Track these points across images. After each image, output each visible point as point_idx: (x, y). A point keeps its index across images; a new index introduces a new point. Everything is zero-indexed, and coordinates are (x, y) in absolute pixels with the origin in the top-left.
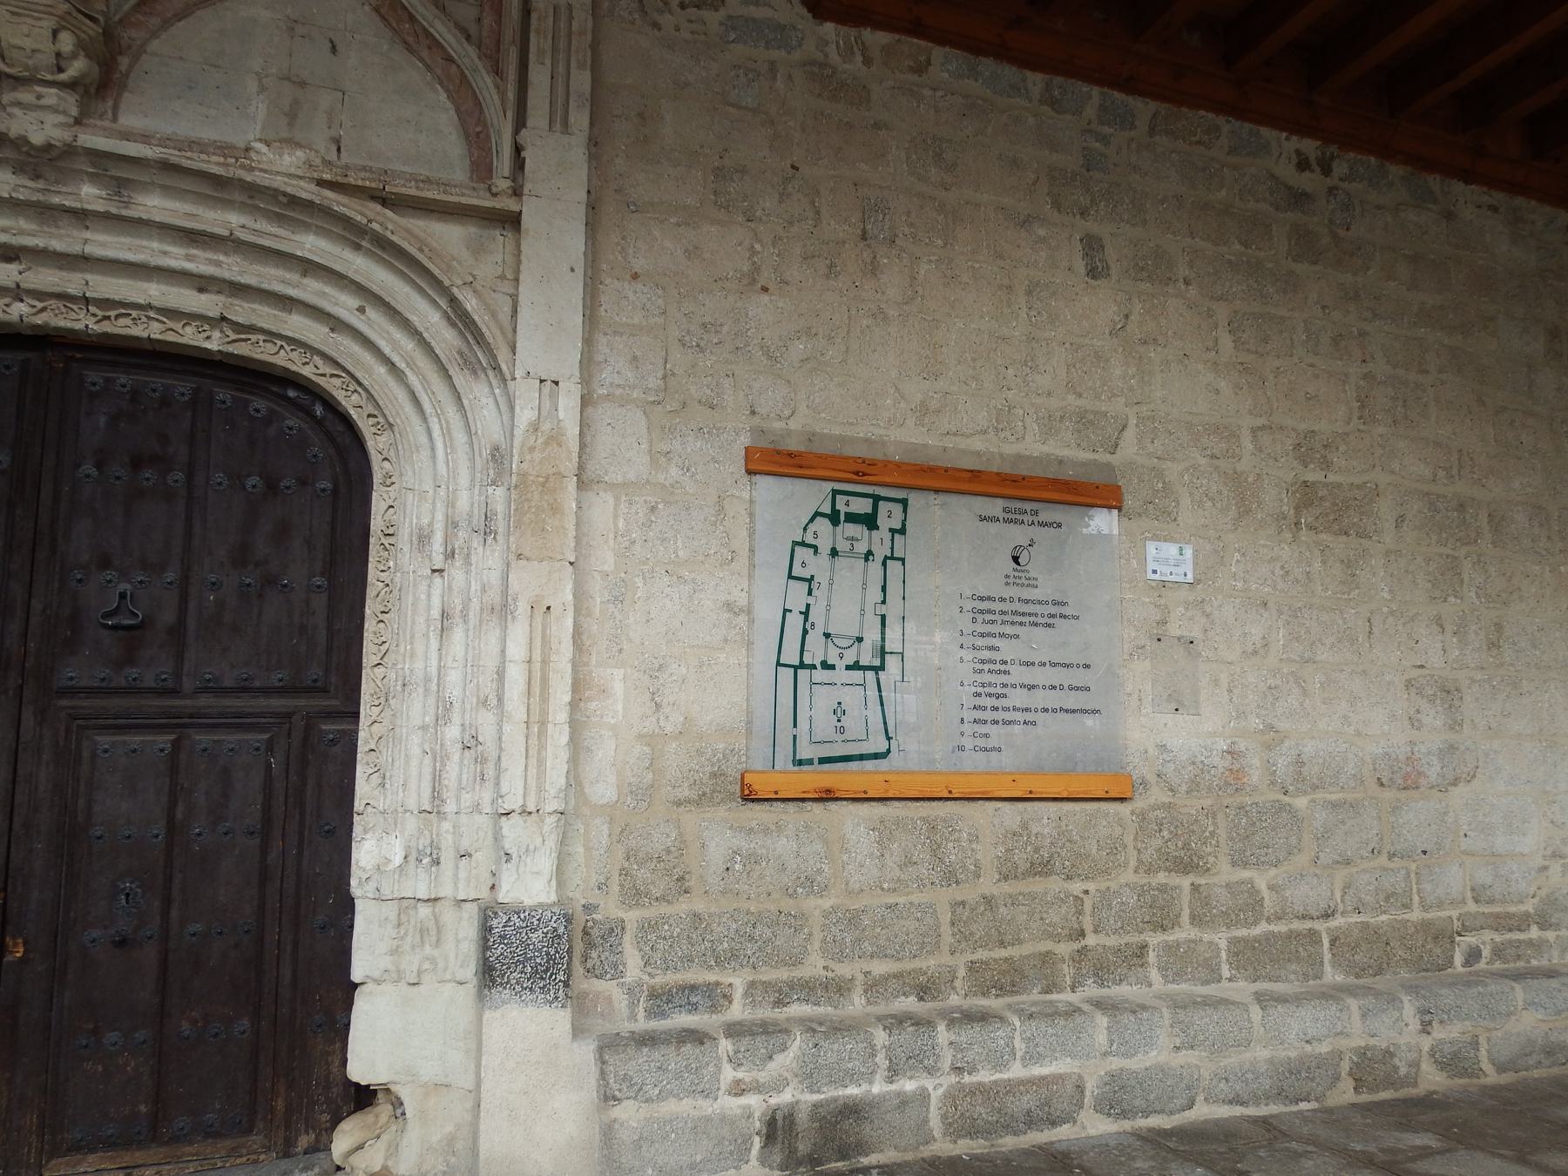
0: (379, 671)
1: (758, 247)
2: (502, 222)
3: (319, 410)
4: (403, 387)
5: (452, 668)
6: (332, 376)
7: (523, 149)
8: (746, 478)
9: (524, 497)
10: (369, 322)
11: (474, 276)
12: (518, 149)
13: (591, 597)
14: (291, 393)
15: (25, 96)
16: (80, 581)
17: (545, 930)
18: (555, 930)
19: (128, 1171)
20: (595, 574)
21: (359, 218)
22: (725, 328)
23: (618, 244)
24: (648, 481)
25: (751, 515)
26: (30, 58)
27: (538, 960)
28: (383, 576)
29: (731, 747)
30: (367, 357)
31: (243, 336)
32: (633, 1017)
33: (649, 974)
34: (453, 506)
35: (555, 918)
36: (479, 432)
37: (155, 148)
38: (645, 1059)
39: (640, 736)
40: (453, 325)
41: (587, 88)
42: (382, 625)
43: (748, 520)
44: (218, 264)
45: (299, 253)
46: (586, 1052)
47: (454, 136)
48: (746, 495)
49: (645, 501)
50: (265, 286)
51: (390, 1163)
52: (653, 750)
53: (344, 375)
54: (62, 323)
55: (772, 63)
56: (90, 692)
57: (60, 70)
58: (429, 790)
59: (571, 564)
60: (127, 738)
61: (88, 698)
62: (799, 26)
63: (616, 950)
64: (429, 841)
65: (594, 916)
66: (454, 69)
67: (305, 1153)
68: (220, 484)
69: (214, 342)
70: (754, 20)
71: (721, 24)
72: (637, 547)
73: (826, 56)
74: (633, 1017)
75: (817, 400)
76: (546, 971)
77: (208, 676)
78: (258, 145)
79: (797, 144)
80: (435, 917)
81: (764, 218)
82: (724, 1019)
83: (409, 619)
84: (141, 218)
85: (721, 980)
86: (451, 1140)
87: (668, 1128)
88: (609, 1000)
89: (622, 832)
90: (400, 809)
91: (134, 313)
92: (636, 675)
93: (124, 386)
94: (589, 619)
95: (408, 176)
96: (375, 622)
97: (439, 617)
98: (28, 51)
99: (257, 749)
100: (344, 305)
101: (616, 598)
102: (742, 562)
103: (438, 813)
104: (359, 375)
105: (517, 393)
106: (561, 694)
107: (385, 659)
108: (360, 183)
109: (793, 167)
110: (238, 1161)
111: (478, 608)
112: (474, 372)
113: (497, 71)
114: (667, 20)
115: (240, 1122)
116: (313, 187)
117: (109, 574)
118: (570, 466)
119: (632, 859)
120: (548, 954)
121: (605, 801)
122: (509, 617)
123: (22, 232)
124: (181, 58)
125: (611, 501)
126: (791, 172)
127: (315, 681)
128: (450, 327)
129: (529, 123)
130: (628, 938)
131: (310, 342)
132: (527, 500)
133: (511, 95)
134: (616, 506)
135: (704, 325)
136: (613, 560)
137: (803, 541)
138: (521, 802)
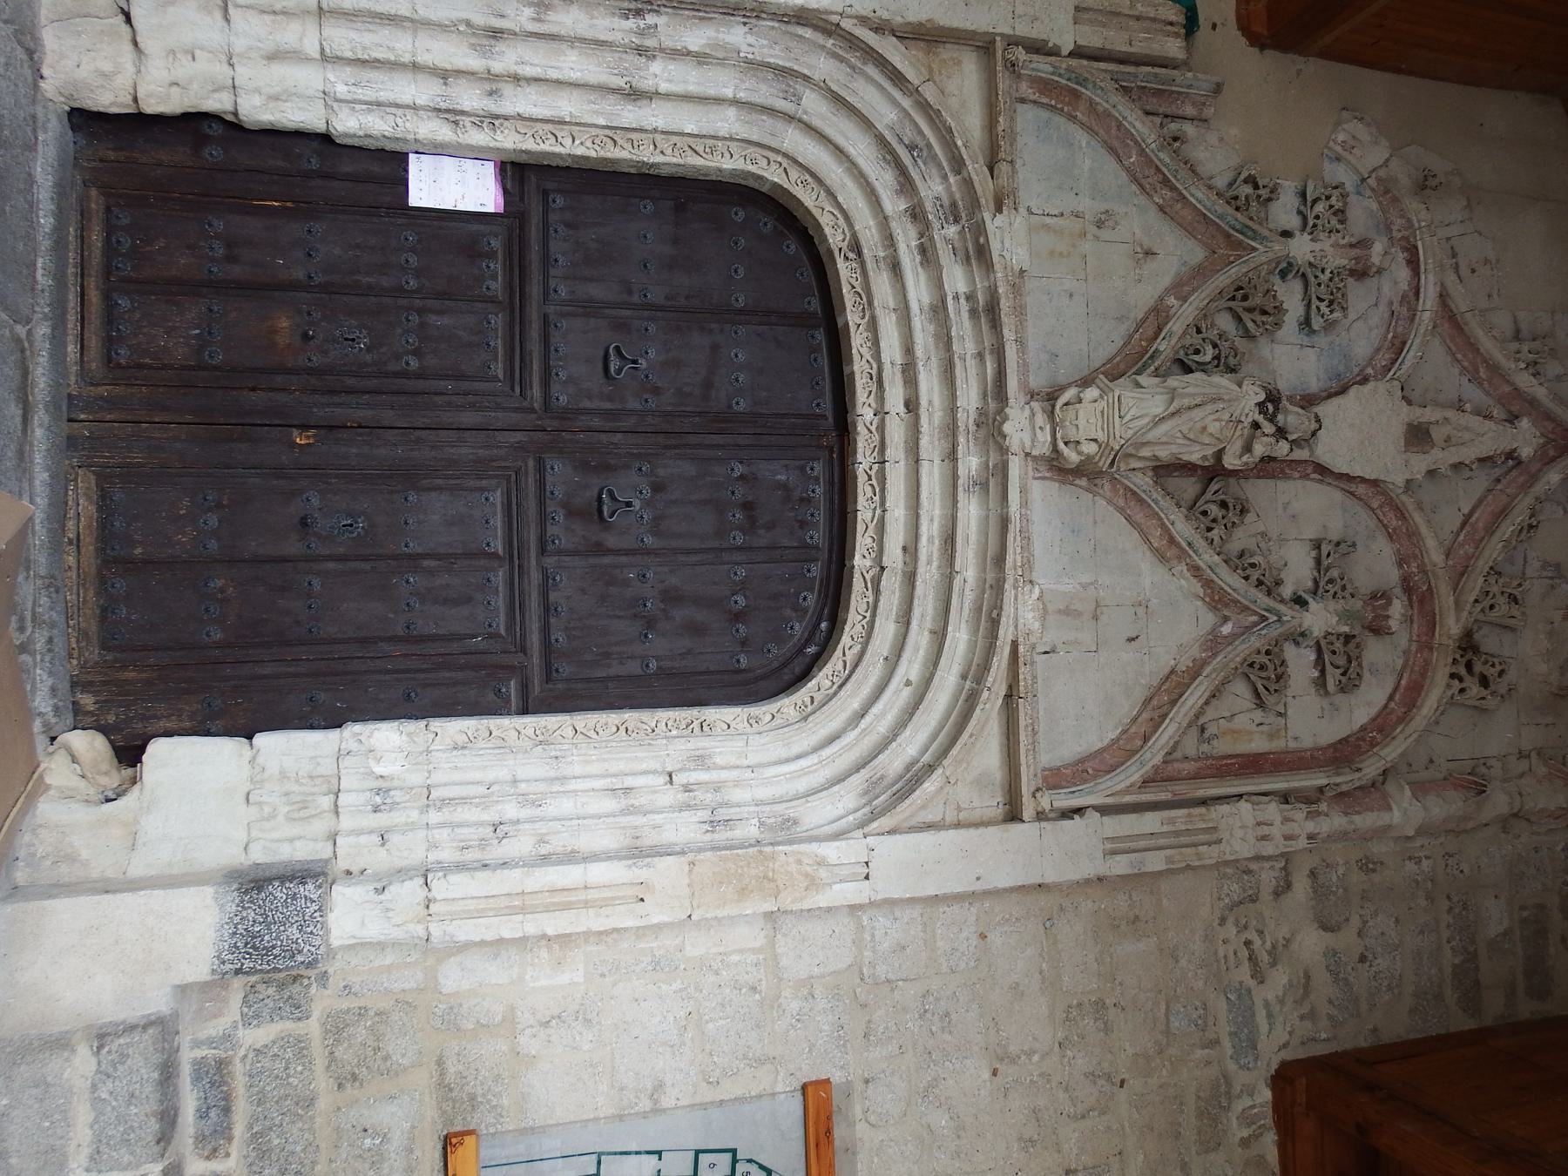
0: (569, 732)
1: (1036, 1058)
2: (1011, 801)
3: (811, 650)
4: (843, 725)
5: (575, 802)
6: (845, 662)
7: (1082, 816)
8: (798, 1086)
9: (751, 860)
10: (898, 692)
11: (956, 783)
12: (1079, 811)
13: (656, 938)
14: (824, 625)
15: (1040, 419)
16: (640, 469)
17: (300, 941)
18: (300, 952)
19: (75, 542)
20: (681, 938)
21: (990, 679)
22: (947, 1037)
23: (1011, 915)
24: (781, 979)
25: (760, 1097)
26: (1070, 423)
27: (267, 938)
28: (662, 726)
29: (504, 1113)
30: (866, 691)
31: (869, 585)
32: (197, 1044)
33: (246, 1056)
34: (735, 786)
35: (313, 949)
36: (809, 805)
37: (1018, 512)
38: (145, 1077)
39: (512, 1009)
40: (908, 768)
41: (1150, 868)
42: (615, 729)
43: (753, 1094)
44: (929, 563)
45: (950, 629)
46: (158, 1002)
47: (1079, 749)
48: (780, 1088)
49: (760, 980)
50: (916, 602)
51: (52, 792)
52: (497, 1025)
53: (847, 672)
54: (860, 445)
55: (1216, 1042)
56: (541, 484)
57: (1066, 443)
58: (451, 796)
59: (690, 916)
60: (499, 515)
61: (536, 481)
62: (1259, 1063)
63: (276, 1014)
64: (398, 800)
65: (315, 985)
66: (1140, 743)
67: (74, 703)
68: (736, 574)
69: (861, 561)
70: (1253, 1015)
71: (1241, 983)
72: (712, 978)
73: (1239, 1097)
74: (197, 1044)
75: (890, 1150)
76: (254, 947)
77: (558, 578)
78: (1037, 591)
79: (1146, 1082)
80: (320, 813)
81: (1066, 1060)
82: (187, 1154)
83: (621, 755)
84: (958, 502)
85: (235, 1143)
86: (72, 858)
87: (57, 1117)
88: (218, 1014)
89: (407, 1003)
90: (431, 767)
91: (877, 498)
92: (579, 996)
93: (813, 491)
94: (633, 938)
95: (1035, 715)
96: (617, 722)
97: (625, 786)
98: (1076, 422)
99: (490, 626)
100: (911, 668)
101: (658, 963)
102: (710, 1095)
103: (428, 806)
104: (848, 686)
105: (852, 842)
106: (553, 924)
107: (581, 736)
108: (1021, 677)
109: (1122, 1083)
110: (73, 640)
111: (637, 824)
112: (866, 792)
113: (1146, 782)
114: (1231, 930)
115: (116, 639)
116: (1010, 638)
117: (648, 493)
118: (787, 901)
119: (377, 1019)
120: (274, 947)
121: (441, 980)
122: (630, 862)
123: (930, 415)
124: (1095, 523)
125: (757, 944)
126: (1117, 1080)
127: (557, 671)
128: (905, 765)
129: (1105, 819)
130: (288, 1025)
131: (872, 641)
132: (749, 864)
133: (1127, 799)
134: (753, 951)
135: (947, 1014)
136: (697, 954)
137: (737, 1161)
138: (439, 897)
